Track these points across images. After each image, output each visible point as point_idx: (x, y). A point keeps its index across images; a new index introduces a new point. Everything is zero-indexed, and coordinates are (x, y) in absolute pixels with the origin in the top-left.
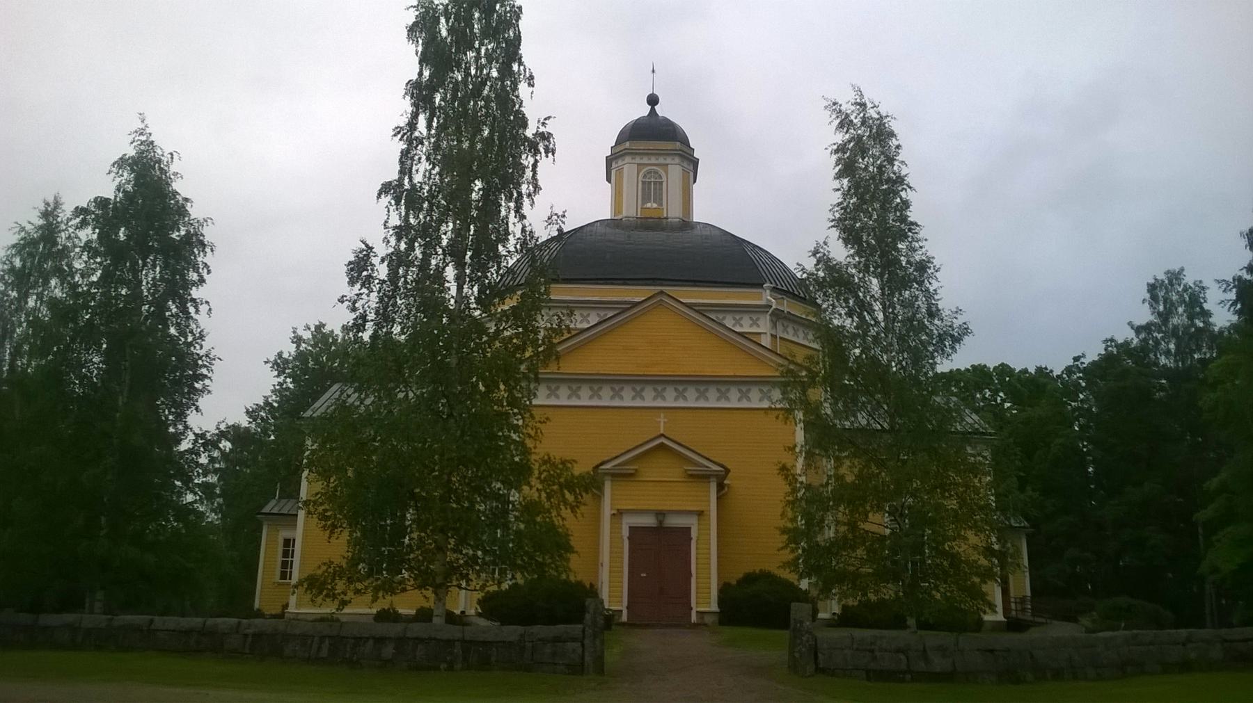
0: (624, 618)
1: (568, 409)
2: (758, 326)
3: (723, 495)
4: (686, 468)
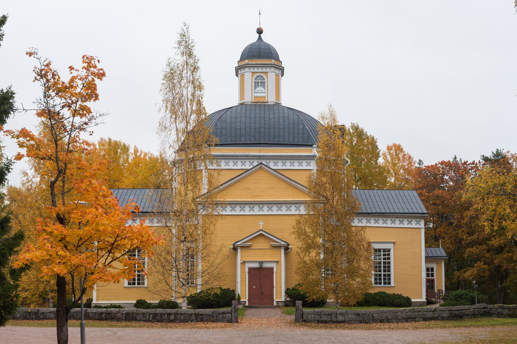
0: (247, 304)
2: (310, 166)
3: (289, 252)
4: (271, 243)
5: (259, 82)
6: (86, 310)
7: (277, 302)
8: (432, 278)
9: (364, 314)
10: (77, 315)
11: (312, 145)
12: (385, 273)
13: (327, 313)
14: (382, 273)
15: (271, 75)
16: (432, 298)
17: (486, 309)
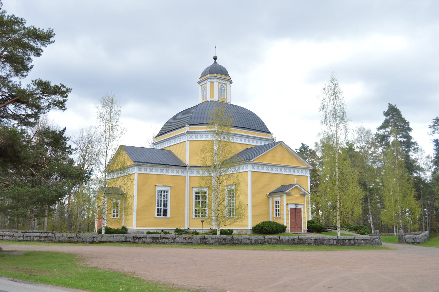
1: (178, 144)
10: (271, 241)
12: (164, 208)
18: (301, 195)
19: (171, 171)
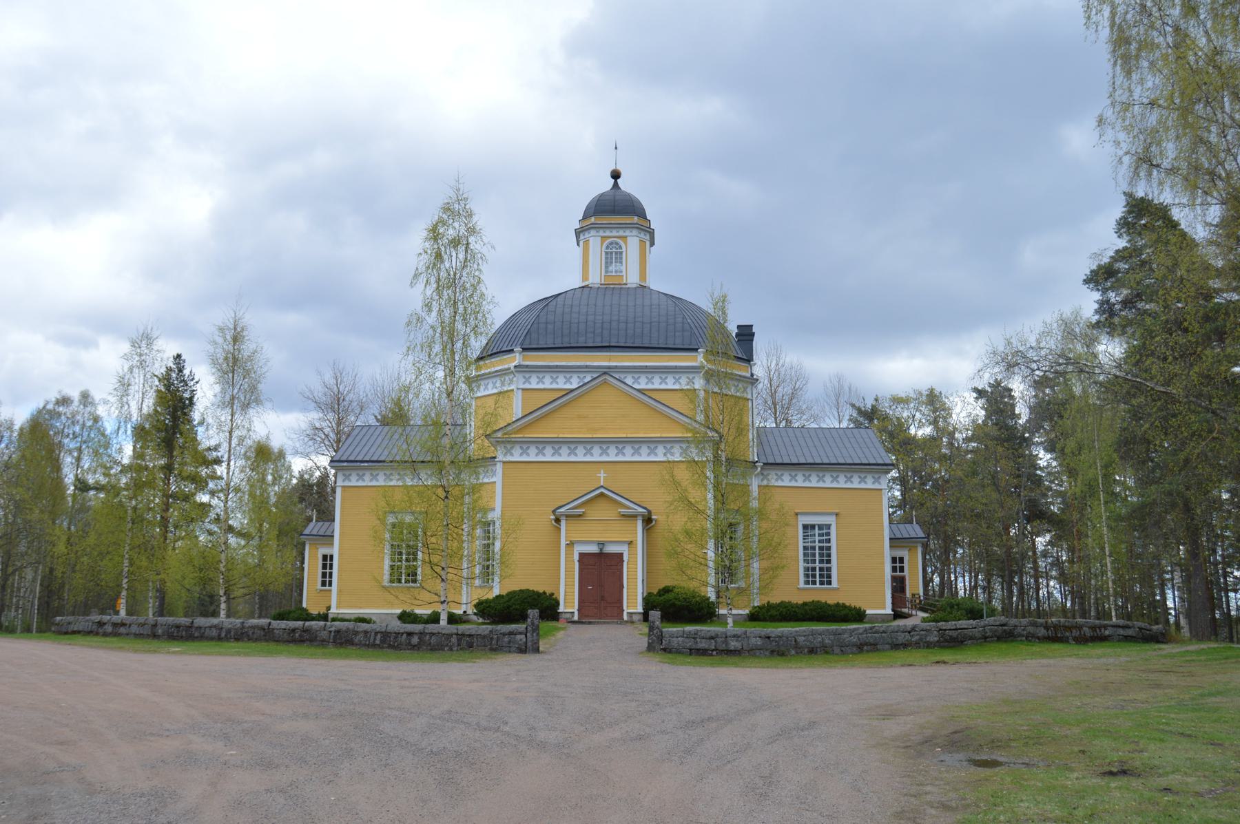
0: (576, 618)
5: (613, 255)
6: (270, 623)
7: (630, 614)
8: (901, 574)
9: (780, 637)
10: (253, 633)
11: (697, 350)
12: (818, 569)
13: (709, 635)
14: (817, 565)
15: (632, 244)
16: (901, 608)
17: (1006, 628)
18: (623, 515)
19: (845, 479)
